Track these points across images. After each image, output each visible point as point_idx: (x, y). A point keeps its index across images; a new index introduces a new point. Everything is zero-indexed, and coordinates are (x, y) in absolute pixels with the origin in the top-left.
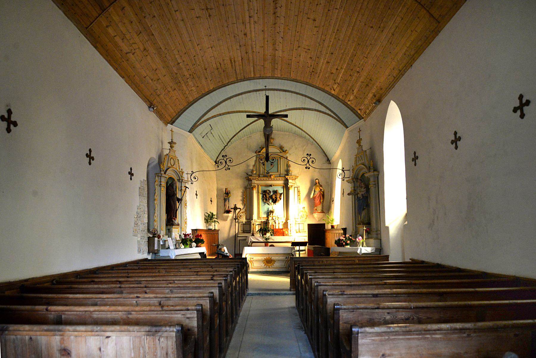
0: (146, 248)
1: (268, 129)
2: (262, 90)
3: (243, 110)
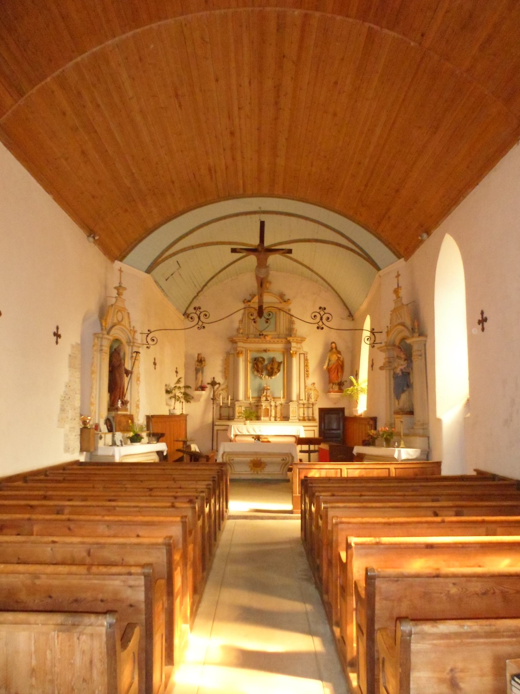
0: (76, 444)
1: (263, 270)
2: (255, 213)
3: (226, 240)
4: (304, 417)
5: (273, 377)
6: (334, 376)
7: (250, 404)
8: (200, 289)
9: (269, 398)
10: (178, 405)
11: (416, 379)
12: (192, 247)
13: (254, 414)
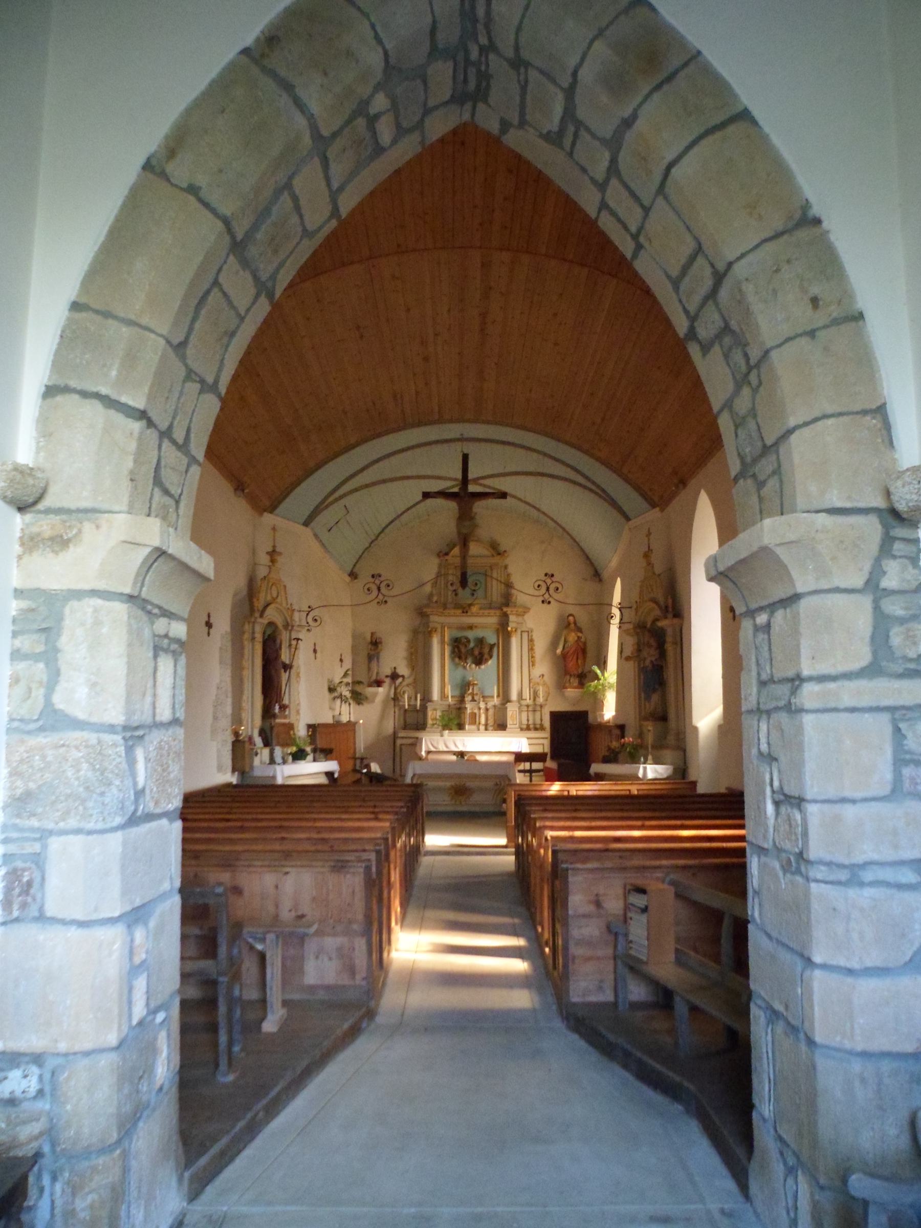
1: (467, 523)
4: (528, 725)
5: (483, 667)
6: (571, 664)
7: (449, 706)
8: (373, 538)
9: (476, 698)
10: (345, 708)
11: (670, 674)
12: (367, 486)
13: (456, 720)
